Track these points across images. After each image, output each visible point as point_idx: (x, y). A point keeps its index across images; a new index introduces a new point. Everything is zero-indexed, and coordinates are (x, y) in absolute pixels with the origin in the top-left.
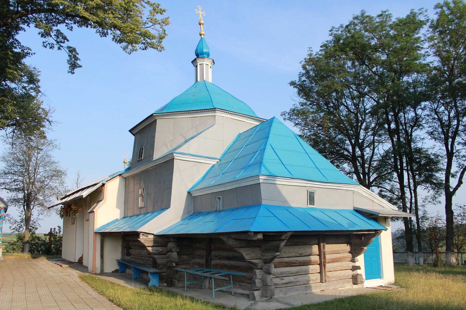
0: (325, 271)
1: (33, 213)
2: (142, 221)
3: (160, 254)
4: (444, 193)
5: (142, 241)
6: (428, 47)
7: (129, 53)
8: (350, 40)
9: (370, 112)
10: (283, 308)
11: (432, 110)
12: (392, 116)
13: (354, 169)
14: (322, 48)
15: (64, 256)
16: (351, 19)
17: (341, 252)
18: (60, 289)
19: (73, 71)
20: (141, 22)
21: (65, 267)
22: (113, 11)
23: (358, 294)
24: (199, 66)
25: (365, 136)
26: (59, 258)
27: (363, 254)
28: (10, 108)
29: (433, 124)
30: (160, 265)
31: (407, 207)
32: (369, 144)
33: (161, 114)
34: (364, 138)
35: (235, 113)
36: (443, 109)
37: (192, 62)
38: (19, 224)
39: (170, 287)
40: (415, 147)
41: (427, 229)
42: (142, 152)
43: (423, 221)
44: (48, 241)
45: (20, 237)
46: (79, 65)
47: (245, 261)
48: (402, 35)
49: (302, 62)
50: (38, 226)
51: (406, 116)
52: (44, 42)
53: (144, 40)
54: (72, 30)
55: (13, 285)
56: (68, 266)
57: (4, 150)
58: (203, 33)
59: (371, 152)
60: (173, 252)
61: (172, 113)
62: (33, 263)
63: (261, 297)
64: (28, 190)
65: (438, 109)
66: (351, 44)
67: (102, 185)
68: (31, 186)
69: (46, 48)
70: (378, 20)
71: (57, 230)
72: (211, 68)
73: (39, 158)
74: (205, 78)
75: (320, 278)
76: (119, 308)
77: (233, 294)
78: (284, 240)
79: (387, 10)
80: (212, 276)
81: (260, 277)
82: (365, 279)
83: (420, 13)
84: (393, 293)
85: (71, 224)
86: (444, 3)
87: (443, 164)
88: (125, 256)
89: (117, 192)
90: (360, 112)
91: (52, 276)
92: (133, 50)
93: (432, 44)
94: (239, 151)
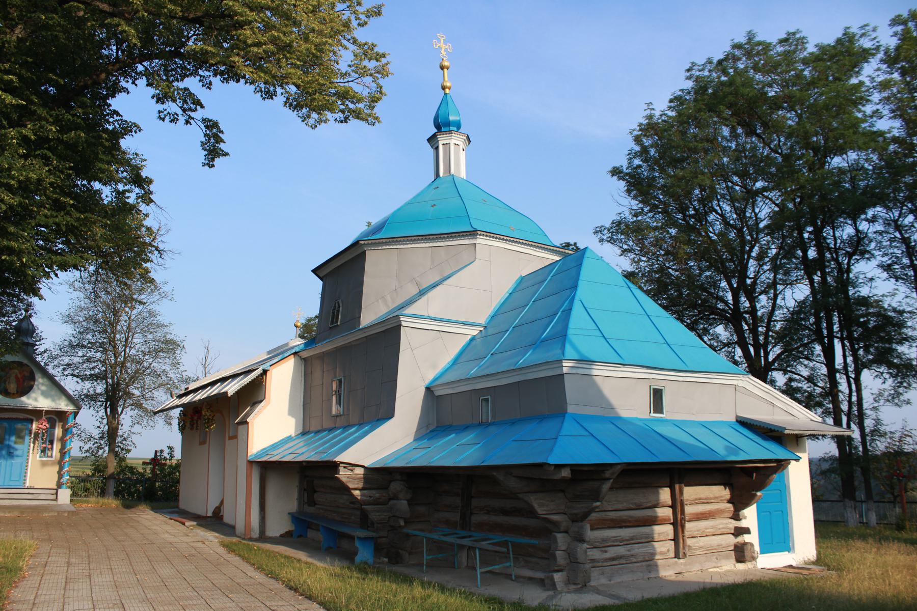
0: (683, 536)
1: (123, 422)
2: (335, 439)
3: (376, 502)
5: (344, 479)
7: (313, 127)
9: (766, 227)
11: (887, 223)
12: (810, 233)
13: (737, 336)
14: (672, 104)
15: (183, 505)
16: (728, 48)
17: (713, 501)
19: (211, 163)
20: (337, 71)
21: (191, 526)
23: (746, 579)
25: (758, 272)
26: (174, 508)
29: (891, 251)
31: (843, 411)
32: (765, 288)
33: (373, 241)
37: (429, 140)
38: (97, 443)
39: (394, 564)
40: (856, 295)
41: (884, 454)
42: (338, 311)
43: (875, 440)
44: (150, 475)
45: (98, 466)
46: (223, 151)
49: (634, 130)
51: (837, 234)
52: (160, 112)
53: (343, 104)
54: (210, 89)
55: (109, 558)
56: (195, 523)
57: (70, 302)
58: (448, 84)
59: (771, 304)
65: (901, 219)
66: (729, 98)
68: (118, 369)
69: (164, 121)
70: (780, 49)
71: (166, 454)
72: (463, 150)
73: (132, 318)
74: (453, 171)
75: (673, 550)
76: (310, 602)
78: (609, 479)
79: (798, 30)
80: (476, 545)
81: (564, 548)
82: (759, 552)
83: (863, 35)
84: (811, 579)
86: (909, 15)
88: (306, 506)
89: (290, 385)
90: (747, 226)
91: (171, 543)
92: (320, 121)
93: (887, 95)
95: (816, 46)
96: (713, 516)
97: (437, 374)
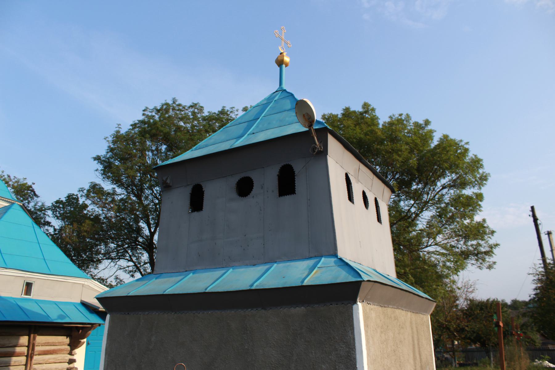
17: (57, 344)
95: (209, 112)
96: (56, 352)
97: (212, 271)
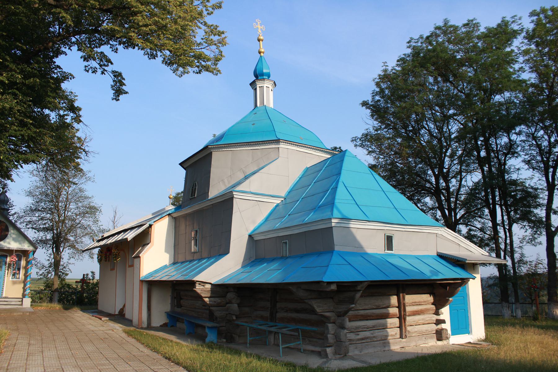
1: (63, 256)
3: (218, 305)
4: (544, 233)
5: (199, 291)
6: (522, 62)
7: (180, 76)
8: (432, 54)
9: (455, 137)
10: (359, 366)
11: (528, 135)
14: (399, 63)
15: (100, 308)
16: (432, 29)
17: (423, 303)
18: (107, 346)
21: (105, 320)
22: (163, 31)
24: (258, 89)
25: (451, 165)
26: (95, 309)
27: (449, 305)
28: (48, 140)
29: (530, 152)
30: (218, 319)
31: (502, 249)
32: (455, 175)
33: (217, 146)
34: (449, 167)
35: (301, 145)
36: (542, 134)
38: (47, 269)
41: (526, 275)
43: (520, 266)
44: (80, 289)
46: (125, 91)
47: (316, 314)
48: (492, 48)
49: (375, 79)
50: (68, 271)
51: (498, 142)
52: (86, 67)
53: (198, 62)
54: (117, 52)
56: (108, 319)
58: (262, 50)
59: (458, 184)
60: (233, 304)
61: (230, 145)
62: (67, 315)
63: (334, 355)
64: (57, 230)
65: (536, 133)
67: (149, 226)
68: (60, 224)
69: (88, 72)
70: (464, 30)
71: (90, 276)
73: (69, 193)
74: (265, 103)
75: (399, 333)
77: (302, 350)
78: (359, 291)
79: (474, 18)
81: (332, 332)
82: (451, 335)
83: (513, 22)
85: (110, 270)
87: (543, 197)
88: (176, 308)
91: (93, 331)
92: (184, 73)
93: (527, 58)
94: (308, 189)
95: (485, 28)
